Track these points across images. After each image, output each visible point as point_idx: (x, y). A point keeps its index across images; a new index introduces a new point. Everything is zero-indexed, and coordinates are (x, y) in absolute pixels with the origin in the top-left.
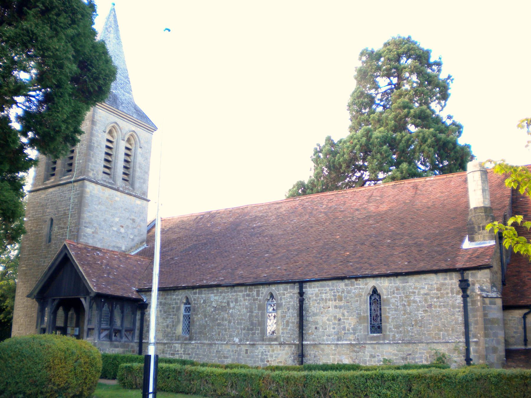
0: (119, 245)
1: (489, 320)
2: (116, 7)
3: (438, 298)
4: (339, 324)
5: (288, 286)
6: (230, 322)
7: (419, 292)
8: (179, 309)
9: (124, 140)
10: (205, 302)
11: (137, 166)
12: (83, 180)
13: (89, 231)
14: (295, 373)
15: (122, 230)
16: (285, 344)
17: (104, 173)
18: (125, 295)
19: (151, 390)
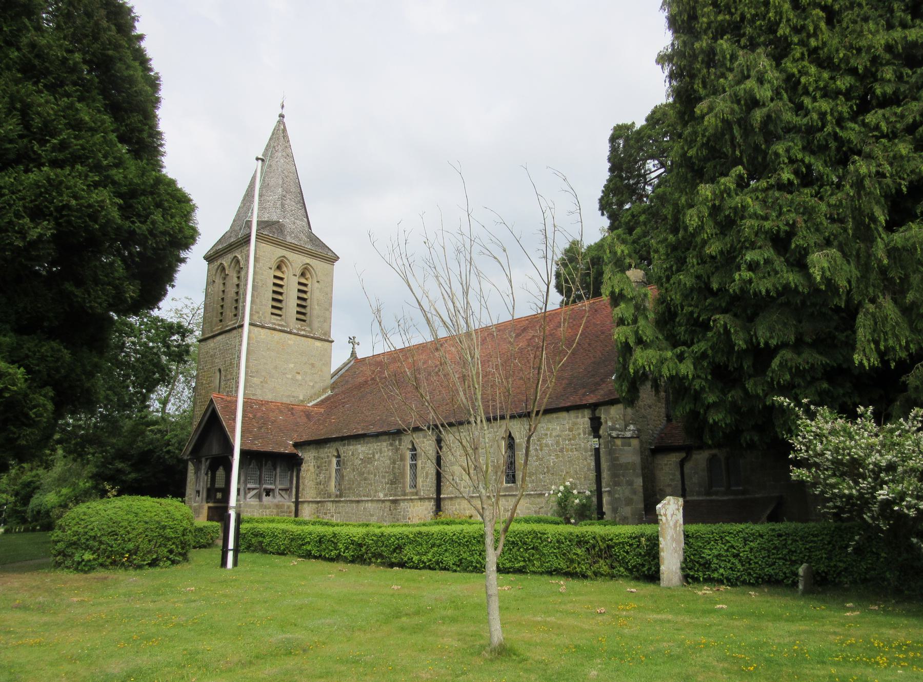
0: (295, 394)
1: (621, 465)
2: (285, 120)
3: (570, 440)
6: (375, 476)
7: (551, 434)
8: (330, 462)
9: (295, 275)
10: (353, 455)
11: (315, 303)
14: (551, 529)
15: (299, 377)
17: (272, 314)
19: (231, 545)
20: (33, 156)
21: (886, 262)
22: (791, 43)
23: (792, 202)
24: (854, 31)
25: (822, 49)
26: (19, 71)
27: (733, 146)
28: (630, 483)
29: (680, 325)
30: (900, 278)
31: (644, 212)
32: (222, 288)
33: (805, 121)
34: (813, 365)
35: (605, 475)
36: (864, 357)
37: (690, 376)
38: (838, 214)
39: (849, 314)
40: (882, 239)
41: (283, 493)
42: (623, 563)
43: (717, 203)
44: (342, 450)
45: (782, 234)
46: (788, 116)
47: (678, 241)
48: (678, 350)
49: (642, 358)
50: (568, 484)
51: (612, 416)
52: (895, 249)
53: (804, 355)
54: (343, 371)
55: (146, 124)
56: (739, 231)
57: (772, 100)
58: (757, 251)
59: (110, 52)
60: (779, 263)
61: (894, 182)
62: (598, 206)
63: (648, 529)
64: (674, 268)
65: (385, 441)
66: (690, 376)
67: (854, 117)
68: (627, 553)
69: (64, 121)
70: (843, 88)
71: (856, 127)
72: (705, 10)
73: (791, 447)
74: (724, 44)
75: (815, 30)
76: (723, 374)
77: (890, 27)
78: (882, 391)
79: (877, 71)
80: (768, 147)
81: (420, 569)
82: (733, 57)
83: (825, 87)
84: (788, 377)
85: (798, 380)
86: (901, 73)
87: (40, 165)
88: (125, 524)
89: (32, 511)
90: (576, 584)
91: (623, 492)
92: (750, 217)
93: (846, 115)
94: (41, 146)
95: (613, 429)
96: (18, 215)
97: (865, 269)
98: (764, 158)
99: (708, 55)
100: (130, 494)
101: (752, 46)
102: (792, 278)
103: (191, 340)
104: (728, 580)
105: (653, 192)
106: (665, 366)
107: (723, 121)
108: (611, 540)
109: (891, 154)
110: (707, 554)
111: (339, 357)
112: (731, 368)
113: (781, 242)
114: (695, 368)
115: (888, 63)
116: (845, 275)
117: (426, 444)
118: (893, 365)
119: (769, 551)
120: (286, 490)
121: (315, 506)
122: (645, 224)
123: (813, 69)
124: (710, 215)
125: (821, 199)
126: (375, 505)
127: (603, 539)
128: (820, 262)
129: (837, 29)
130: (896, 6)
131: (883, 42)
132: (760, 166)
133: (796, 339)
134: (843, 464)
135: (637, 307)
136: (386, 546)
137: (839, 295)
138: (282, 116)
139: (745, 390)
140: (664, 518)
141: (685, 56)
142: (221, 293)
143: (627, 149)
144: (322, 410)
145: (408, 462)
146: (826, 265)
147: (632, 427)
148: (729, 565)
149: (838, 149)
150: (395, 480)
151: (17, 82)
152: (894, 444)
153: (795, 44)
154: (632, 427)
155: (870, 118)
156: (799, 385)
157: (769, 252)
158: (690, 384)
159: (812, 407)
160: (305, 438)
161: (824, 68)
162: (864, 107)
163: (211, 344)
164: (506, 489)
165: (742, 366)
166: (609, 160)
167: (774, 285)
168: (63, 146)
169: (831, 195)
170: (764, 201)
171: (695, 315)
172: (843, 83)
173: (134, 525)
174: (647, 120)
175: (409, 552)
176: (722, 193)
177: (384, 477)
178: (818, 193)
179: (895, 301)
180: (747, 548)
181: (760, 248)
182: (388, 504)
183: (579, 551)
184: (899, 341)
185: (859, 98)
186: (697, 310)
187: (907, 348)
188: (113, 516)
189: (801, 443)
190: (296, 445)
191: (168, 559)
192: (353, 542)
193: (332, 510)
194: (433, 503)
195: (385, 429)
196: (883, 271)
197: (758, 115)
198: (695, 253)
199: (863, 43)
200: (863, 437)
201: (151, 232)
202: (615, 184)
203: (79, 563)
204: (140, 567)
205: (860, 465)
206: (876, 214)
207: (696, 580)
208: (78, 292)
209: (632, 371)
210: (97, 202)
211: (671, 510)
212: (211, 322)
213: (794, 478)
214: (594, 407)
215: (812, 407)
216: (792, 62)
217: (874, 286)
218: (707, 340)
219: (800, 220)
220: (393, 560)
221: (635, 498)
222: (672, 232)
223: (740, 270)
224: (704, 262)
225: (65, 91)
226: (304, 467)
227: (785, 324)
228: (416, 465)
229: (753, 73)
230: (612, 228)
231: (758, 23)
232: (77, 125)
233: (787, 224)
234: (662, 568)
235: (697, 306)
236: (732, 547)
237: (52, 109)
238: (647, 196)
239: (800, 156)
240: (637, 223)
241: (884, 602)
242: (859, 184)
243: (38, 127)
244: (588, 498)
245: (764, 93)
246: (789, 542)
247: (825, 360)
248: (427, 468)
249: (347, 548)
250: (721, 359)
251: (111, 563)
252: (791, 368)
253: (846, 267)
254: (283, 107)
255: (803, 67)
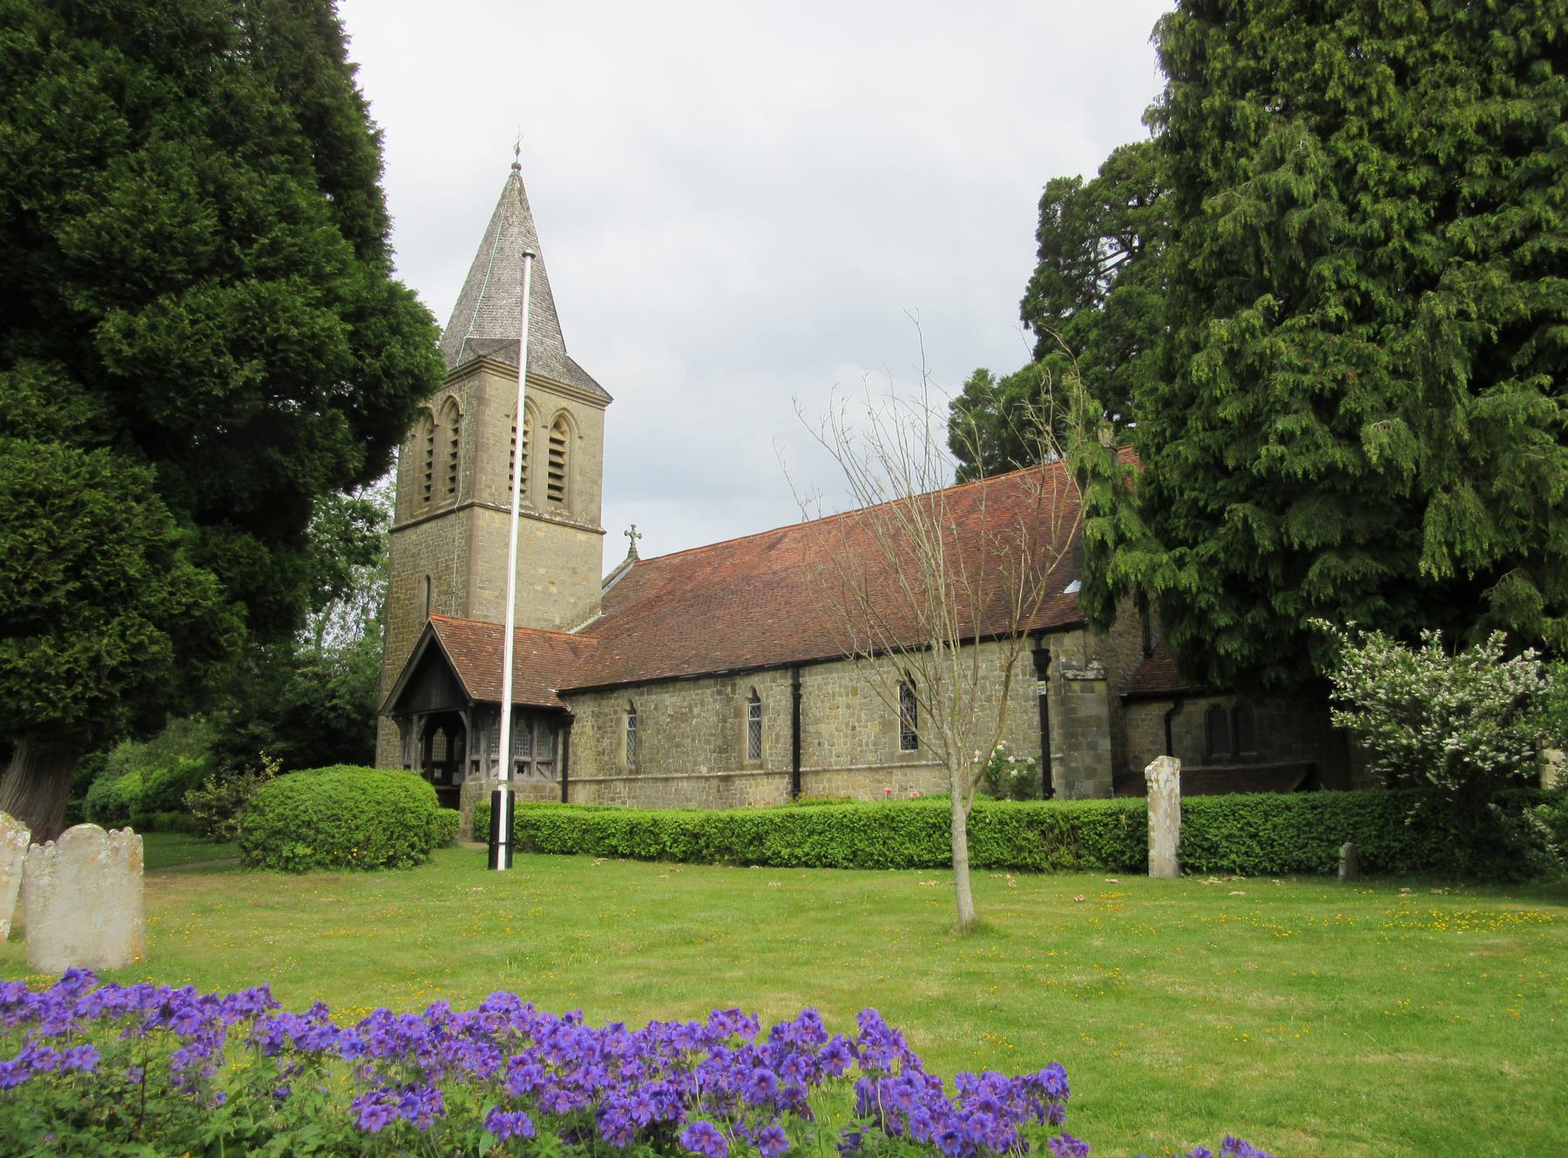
1: (1079, 720)
2: (522, 173)
4: (854, 737)
5: (778, 674)
8: (619, 720)
11: (576, 472)
12: (471, 505)
13: (488, 594)
15: (553, 589)
16: (774, 773)
18: (533, 702)
19: (502, 837)
20: (229, 262)
21: (1466, 437)
22: (1344, 111)
23: (1342, 346)
24: (1434, 98)
25: (1389, 121)
26: (207, 135)
27: (1260, 264)
28: (1093, 747)
29: (1179, 518)
30: (1485, 459)
31: (1096, 325)
32: (427, 447)
33: (1362, 229)
34: (1365, 574)
35: (1056, 735)
36: (1432, 565)
37: (1194, 589)
38: (1405, 366)
39: (1415, 507)
40: (1463, 405)
41: (543, 768)
42: (1096, 850)
43: (1236, 346)
44: (638, 701)
45: (1327, 394)
46: (1339, 222)
47: (1173, 392)
48: (1177, 552)
49: (1126, 563)
50: (1000, 747)
51: (1067, 649)
52: (1480, 419)
53: (1355, 561)
54: (617, 579)
55: (371, 206)
56: (1266, 387)
57: (1316, 195)
58: (1292, 416)
59: (327, 100)
60: (1321, 433)
61: (1481, 325)
62: (1019, 313)
63: (1131, 803)
64: (1168, 433)
65: (708, 687)
66: (1194, 589)
67: (1430, 227)
68: (1100, 835)
69: (273, 209)
70: (1417, 183)
71: (1434, 240)
72: (1219, 50)
73: (1331, 686)
74: (1246, 107)
75: (1379, 95)
76: (1241, 588)
77: (1486, 93)
78: (1454, 610)
79: (1465, 161)
80: (1309, 266)
81: (793, 866)
82: (1261, 127)
83: (1392, 180)
84: (1330, 591)
85: (1343, 596)
86: (1499, 165)
87: (241, 276)
88: (350, 804)
89: (94, 806)
90: (1029, 880)
91: (1082, 759)
92: (1283, 369)
93: (1420, 223)
94: (243, 246)
95: (1068, 667)
96: (217, 352)
97: (1439, 445)
98: (1303, 280)
99: (1223, 119)
100: (346, 763)
101: (1287, 112)
102: (1339, 455)
103: (381, 529)
104: (1242, 868)
105: (1109, 290)
106: (1159, 574)
107: (1245, 227)
108: (1078, 818)
109: (1481, 283)
110: (1213, 834)
111: (613, 557)
112: (1251, 578)
113: (1324, 403)
114: (1201, 578)
115: (1481, 150)
116: (1411, 452)
117: (775, 692)
118: (1471, 575)
119: (1299, 829)
120: (547, 764)
121: (594, 787)
122: (1097, 344)
123: (1375, 154)
124: (1225, 363)
125: (1381, 343)
126: (693, 784)
127: (1066, 817)
128: (1378, 435)
129: (1411, 94)
130: (1495, 64)
131: (1474, 120)
132: (1298, 295)
133: (1343, 538)
134: (1403, 708)
135: (1116, 491)
136: (738, 836)
137: (1402, 481)
138: (517, 167)
139: (1271, 610)
140: (1155, 786)
141: (1187, 118)
142: (426, 455)
143: (1068, 220)
144: (595, 642)
145: (747, 719)
146: (1385, 440)
147: (1095, 664)
148: (1243, 849)
149: (1408, 272)
150: (726, 748)
151: (208, 151)
152: (1468, 681)
153: (1351, 114)
154: (1095, 664)
155: (1455, 230)
156: (1345, 601)
157: (1308, 419)
158: (1194, 599)
159: (1361, 633)
160: (575, 684)
161: (1390, 151)
162: (1447, 207)
163: (411, 535)
164: (903, 758)
165: (1266, 575)
166: (1039, 236)
167: (1314, 465)
168: (275, 247)
169: (1394, 339)
170: (1303, 346)
171: (1201, 503)
172: (1416, 177)
173: (363, 806)
174: (1102, 172)
175: (774, 844)
176: (1243, 332)
177: (708, 742)
178: (1377, 333)
179: (1477, 489)
180: (1269, 825)
181: (1296, 412)
182: (715, 782)
183: (1030, 835)
184: (1480, 543)
185: (1439, 198)
186: (1203, 496)
187: (1490, 553)
188: (332, 793)
189: (1345, 680)
190: (562, 695)
191: (409, 857)
192: (684, 832)
193: (624, 793)
194: (787, 779)
195: (708, 669)
196: (1463, 448)
197: (1296, 219)
198: (1200, 413)
199: (1446, 119)
200: (1428, 670)
201: (387, 372)
202: (1048, 277)
203: (288, 859)
204: (372, 867)
205: (1424, 709)
206: (1455, 372)
207: (1197, 870)
208: (287, 462)
209: (1110, 581)
210: (323, 330)
211: (1164, 774)
212: (411, 501)
213: (1336, 725)
214: (1038, 634)
215: (1361, 633)
216: (1345, 141)
217: (1449, 469)
218: (1219, 539)
219: (1352, 373)
220: (750, 856)
221: (1100, 767)
222: (1162, 378)
223: (1267, 442)
224: (1213, 428)
225: (270, 163)
226: (576, 728)
227: (1328, 518)
228: (759, 724)
229: (1289, 157)
230: (1039, 353)
231: (1297, 76)
232: (290, 216)
233: (1335, 380)
234: (1152, 853)
235: (1203, 491)
236: (1249, 824)
237: (260, 192)
238: (1101, 298)
239: (1353, 280)
240: (1085, 342)
241: (1451, 886)
242: (1434, 328)
243: (239, 220)
244: (1030, 768)
245: (1304, 187)
246: (1327, 816)
247: (1382, 568)
248: (777, 724)
249: (675, 841)
250: (1237, 565)
251: (332, 862)
252: (1335, 579)
253: (1413, 443)
254: (518, 152)
255: (1361, 149)
